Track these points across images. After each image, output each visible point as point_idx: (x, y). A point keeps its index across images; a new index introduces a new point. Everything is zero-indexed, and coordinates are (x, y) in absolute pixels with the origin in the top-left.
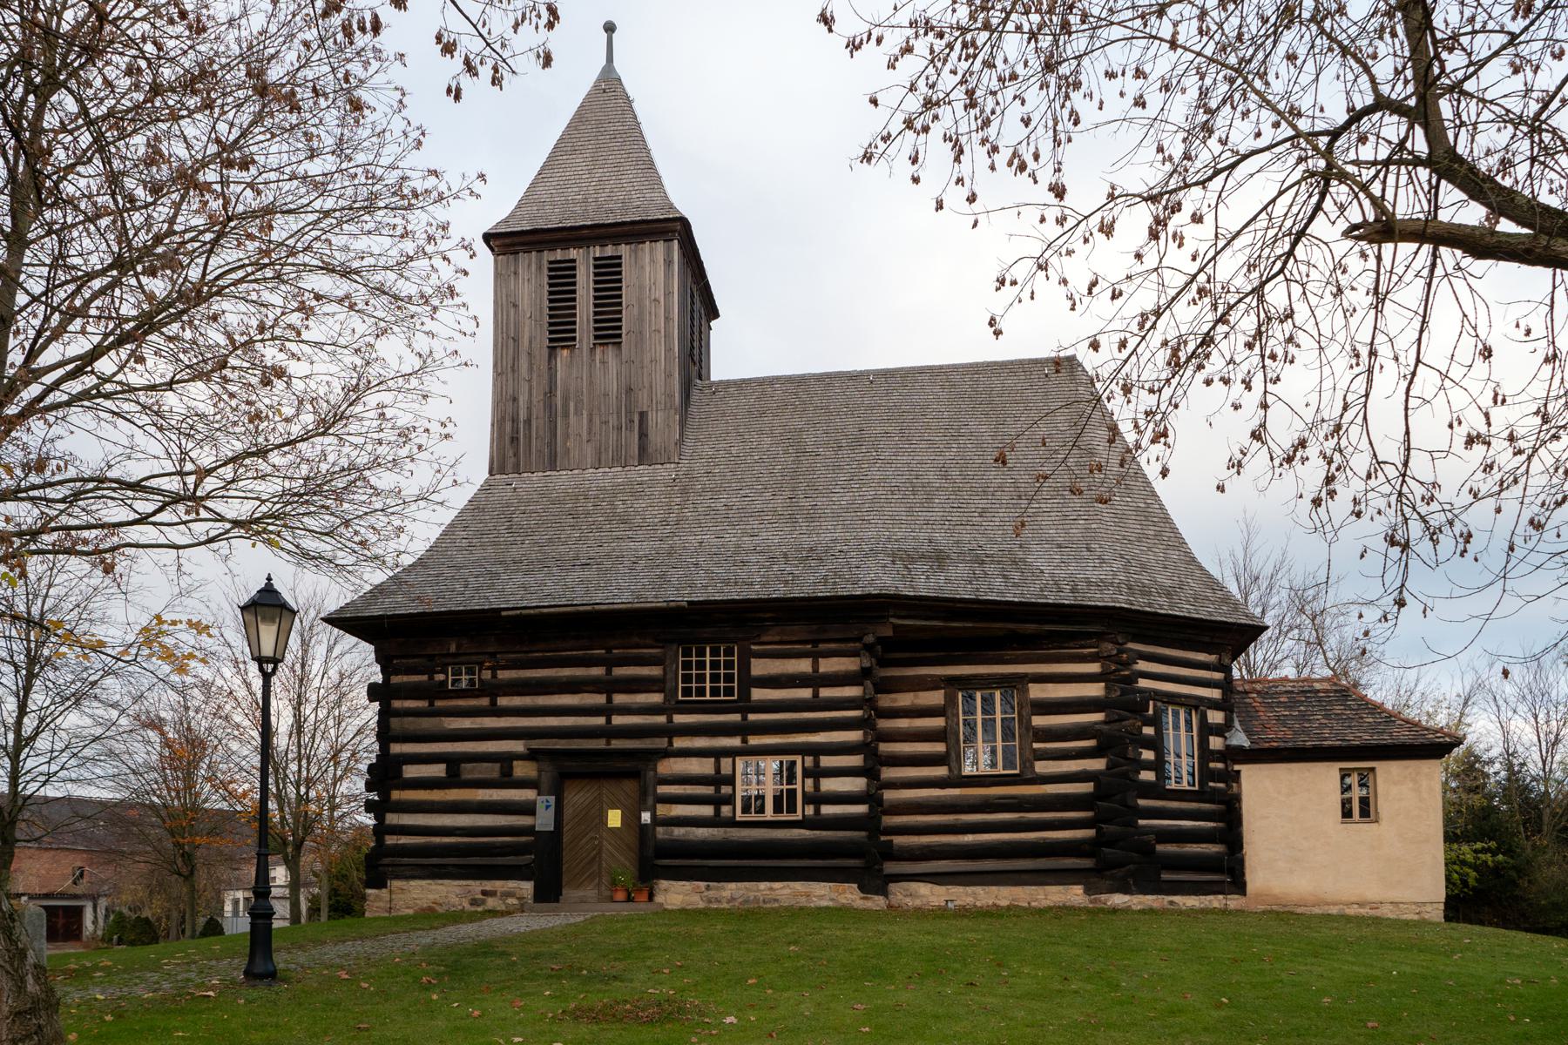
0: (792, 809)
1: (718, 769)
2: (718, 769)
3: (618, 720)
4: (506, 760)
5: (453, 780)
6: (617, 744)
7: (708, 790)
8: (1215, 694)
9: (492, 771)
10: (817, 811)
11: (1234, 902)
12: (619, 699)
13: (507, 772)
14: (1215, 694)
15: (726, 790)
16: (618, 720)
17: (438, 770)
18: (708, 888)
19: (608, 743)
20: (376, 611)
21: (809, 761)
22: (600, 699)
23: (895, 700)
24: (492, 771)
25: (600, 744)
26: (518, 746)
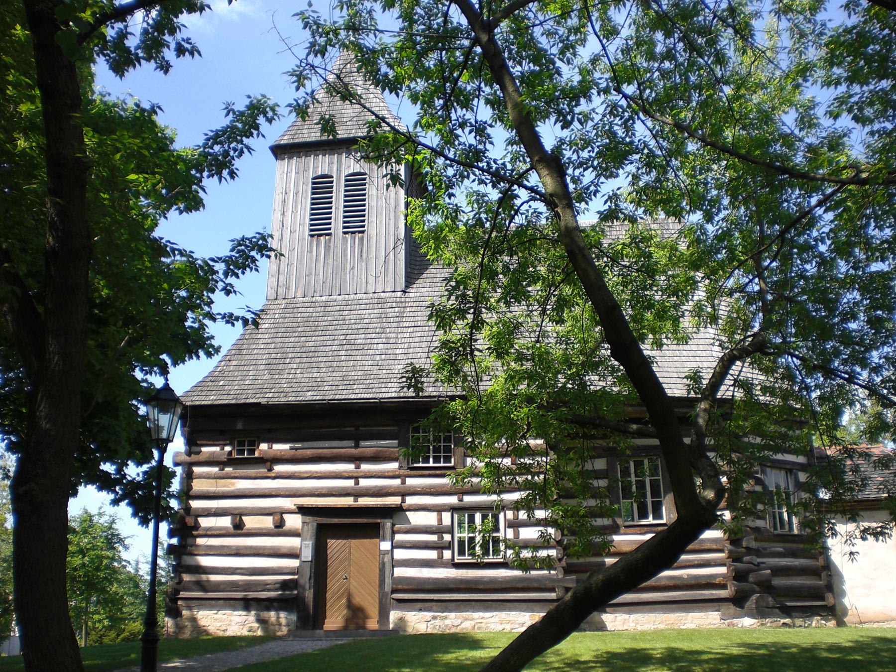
0: (496, 552)
1: (440, 520)
2: (440, 520)
3: (363, 483)
4: (279, 515)
5: (238, 528)
6: (364, 501)
7: (434, 538)
8: (801, 459)
9: (268, 522)
10: (517, 554)
11: (815, 632)
12: (365, 467)
13: (280, 524)
14: (801, 459)
15: (447, 537)
16: (363, 483)
17: (226, 522)
18: (434, 618)
19: (356, 501)
20: (211, 399)
21: (510, 514)
22: (350, 467)
23: (233, 484)
24: (268, 522)
25: (348, 501)
26: (288, 503)
